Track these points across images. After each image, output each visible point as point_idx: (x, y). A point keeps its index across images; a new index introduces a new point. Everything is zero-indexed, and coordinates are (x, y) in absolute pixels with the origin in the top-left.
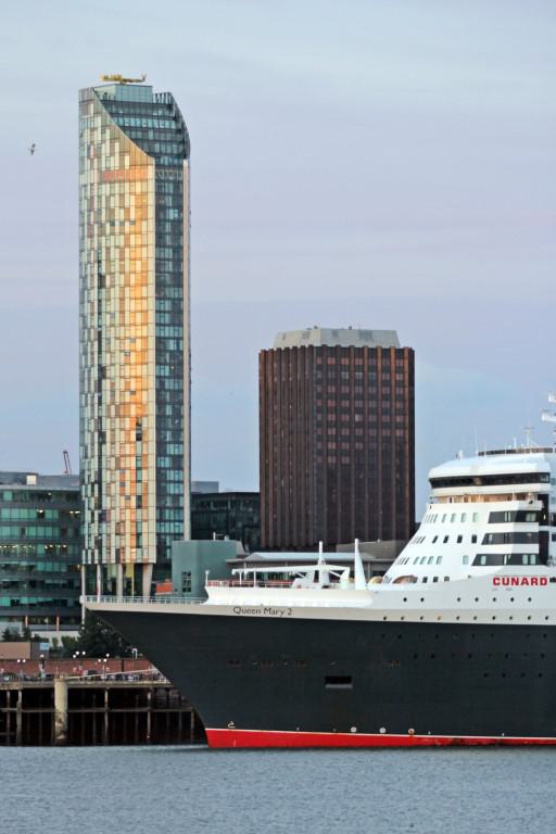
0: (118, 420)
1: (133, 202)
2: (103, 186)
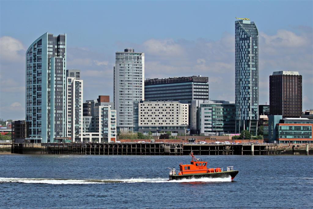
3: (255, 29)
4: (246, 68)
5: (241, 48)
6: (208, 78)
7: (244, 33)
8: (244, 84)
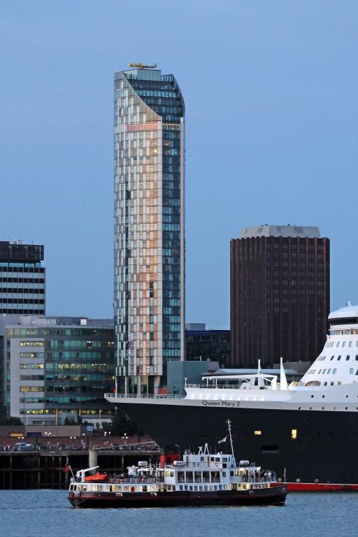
0: (138, 284)
1: (148, 145)
2: (129, 134)
3: (174, 96)
4: (138, 267)
5: (129, 155)
6: (42, 247)
7: (138, 108)
8: (138, 300)
